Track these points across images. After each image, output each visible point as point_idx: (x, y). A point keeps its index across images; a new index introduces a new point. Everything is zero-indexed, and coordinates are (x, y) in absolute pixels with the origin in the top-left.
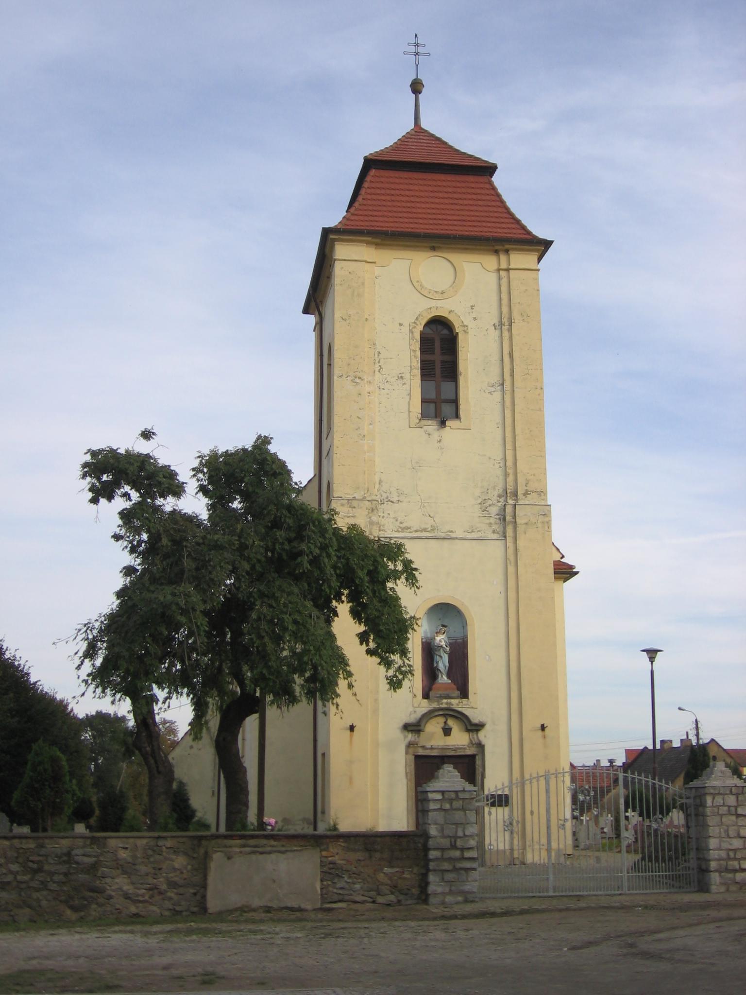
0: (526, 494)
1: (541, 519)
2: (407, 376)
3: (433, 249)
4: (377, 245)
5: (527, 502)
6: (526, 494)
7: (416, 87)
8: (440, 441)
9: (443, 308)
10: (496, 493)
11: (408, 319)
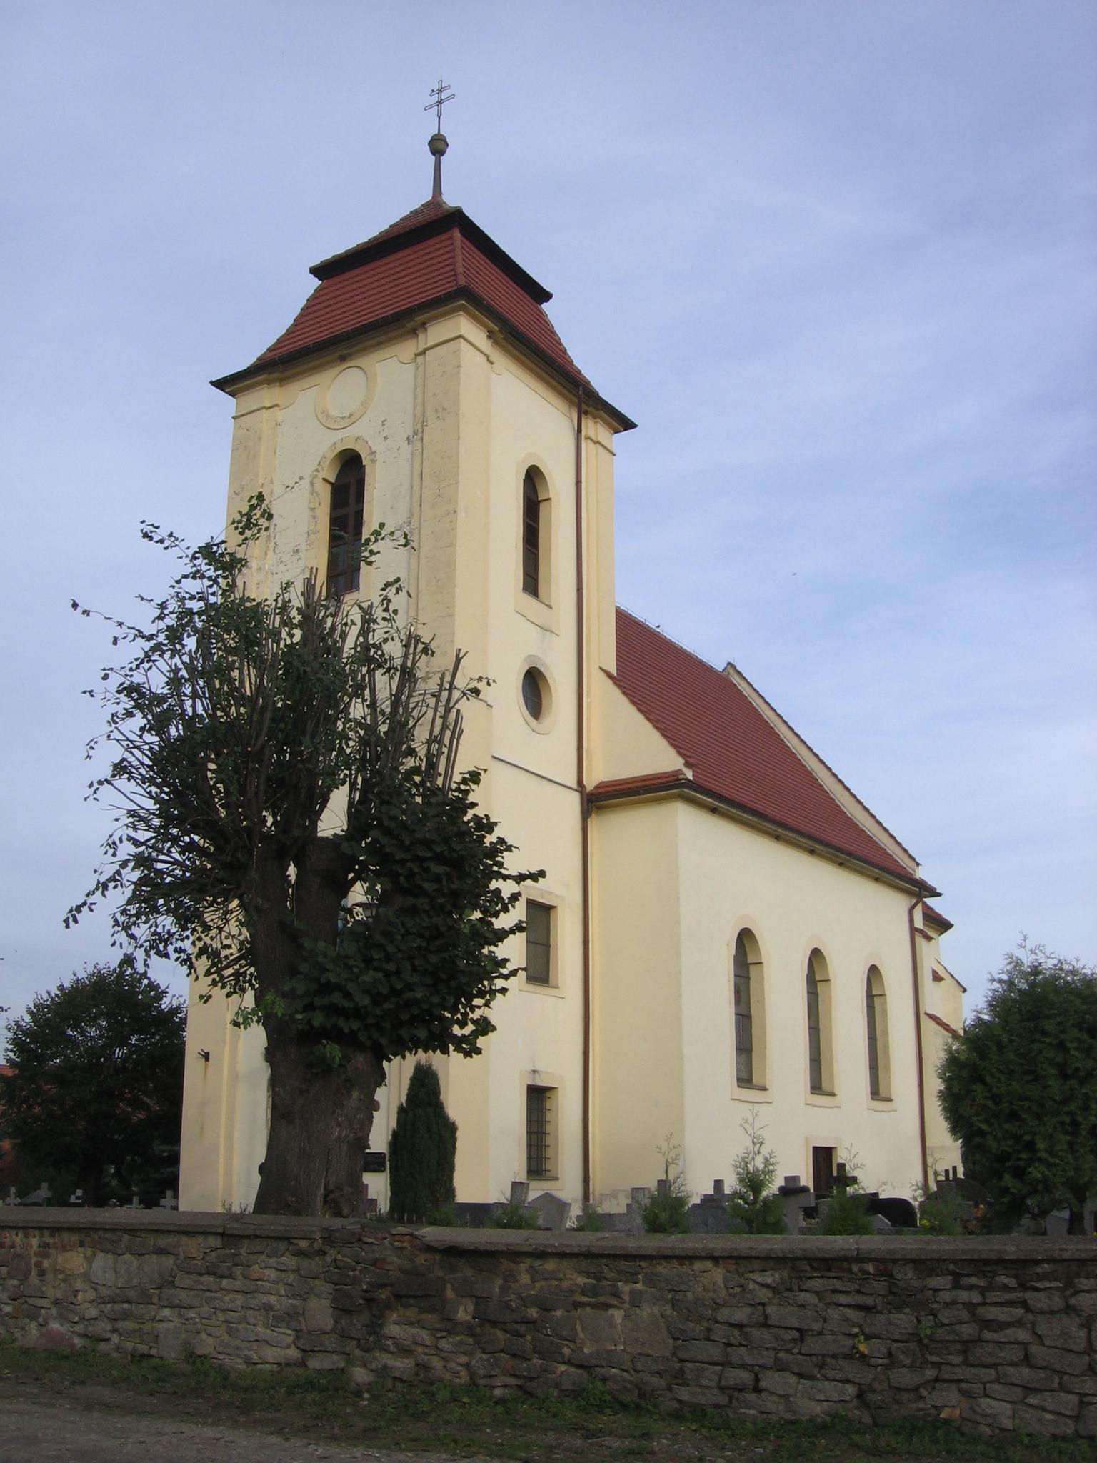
2: (303, 547)
3: (343, 359)
4: (282, 381)
7: (438, 146)
9: (345, 439)
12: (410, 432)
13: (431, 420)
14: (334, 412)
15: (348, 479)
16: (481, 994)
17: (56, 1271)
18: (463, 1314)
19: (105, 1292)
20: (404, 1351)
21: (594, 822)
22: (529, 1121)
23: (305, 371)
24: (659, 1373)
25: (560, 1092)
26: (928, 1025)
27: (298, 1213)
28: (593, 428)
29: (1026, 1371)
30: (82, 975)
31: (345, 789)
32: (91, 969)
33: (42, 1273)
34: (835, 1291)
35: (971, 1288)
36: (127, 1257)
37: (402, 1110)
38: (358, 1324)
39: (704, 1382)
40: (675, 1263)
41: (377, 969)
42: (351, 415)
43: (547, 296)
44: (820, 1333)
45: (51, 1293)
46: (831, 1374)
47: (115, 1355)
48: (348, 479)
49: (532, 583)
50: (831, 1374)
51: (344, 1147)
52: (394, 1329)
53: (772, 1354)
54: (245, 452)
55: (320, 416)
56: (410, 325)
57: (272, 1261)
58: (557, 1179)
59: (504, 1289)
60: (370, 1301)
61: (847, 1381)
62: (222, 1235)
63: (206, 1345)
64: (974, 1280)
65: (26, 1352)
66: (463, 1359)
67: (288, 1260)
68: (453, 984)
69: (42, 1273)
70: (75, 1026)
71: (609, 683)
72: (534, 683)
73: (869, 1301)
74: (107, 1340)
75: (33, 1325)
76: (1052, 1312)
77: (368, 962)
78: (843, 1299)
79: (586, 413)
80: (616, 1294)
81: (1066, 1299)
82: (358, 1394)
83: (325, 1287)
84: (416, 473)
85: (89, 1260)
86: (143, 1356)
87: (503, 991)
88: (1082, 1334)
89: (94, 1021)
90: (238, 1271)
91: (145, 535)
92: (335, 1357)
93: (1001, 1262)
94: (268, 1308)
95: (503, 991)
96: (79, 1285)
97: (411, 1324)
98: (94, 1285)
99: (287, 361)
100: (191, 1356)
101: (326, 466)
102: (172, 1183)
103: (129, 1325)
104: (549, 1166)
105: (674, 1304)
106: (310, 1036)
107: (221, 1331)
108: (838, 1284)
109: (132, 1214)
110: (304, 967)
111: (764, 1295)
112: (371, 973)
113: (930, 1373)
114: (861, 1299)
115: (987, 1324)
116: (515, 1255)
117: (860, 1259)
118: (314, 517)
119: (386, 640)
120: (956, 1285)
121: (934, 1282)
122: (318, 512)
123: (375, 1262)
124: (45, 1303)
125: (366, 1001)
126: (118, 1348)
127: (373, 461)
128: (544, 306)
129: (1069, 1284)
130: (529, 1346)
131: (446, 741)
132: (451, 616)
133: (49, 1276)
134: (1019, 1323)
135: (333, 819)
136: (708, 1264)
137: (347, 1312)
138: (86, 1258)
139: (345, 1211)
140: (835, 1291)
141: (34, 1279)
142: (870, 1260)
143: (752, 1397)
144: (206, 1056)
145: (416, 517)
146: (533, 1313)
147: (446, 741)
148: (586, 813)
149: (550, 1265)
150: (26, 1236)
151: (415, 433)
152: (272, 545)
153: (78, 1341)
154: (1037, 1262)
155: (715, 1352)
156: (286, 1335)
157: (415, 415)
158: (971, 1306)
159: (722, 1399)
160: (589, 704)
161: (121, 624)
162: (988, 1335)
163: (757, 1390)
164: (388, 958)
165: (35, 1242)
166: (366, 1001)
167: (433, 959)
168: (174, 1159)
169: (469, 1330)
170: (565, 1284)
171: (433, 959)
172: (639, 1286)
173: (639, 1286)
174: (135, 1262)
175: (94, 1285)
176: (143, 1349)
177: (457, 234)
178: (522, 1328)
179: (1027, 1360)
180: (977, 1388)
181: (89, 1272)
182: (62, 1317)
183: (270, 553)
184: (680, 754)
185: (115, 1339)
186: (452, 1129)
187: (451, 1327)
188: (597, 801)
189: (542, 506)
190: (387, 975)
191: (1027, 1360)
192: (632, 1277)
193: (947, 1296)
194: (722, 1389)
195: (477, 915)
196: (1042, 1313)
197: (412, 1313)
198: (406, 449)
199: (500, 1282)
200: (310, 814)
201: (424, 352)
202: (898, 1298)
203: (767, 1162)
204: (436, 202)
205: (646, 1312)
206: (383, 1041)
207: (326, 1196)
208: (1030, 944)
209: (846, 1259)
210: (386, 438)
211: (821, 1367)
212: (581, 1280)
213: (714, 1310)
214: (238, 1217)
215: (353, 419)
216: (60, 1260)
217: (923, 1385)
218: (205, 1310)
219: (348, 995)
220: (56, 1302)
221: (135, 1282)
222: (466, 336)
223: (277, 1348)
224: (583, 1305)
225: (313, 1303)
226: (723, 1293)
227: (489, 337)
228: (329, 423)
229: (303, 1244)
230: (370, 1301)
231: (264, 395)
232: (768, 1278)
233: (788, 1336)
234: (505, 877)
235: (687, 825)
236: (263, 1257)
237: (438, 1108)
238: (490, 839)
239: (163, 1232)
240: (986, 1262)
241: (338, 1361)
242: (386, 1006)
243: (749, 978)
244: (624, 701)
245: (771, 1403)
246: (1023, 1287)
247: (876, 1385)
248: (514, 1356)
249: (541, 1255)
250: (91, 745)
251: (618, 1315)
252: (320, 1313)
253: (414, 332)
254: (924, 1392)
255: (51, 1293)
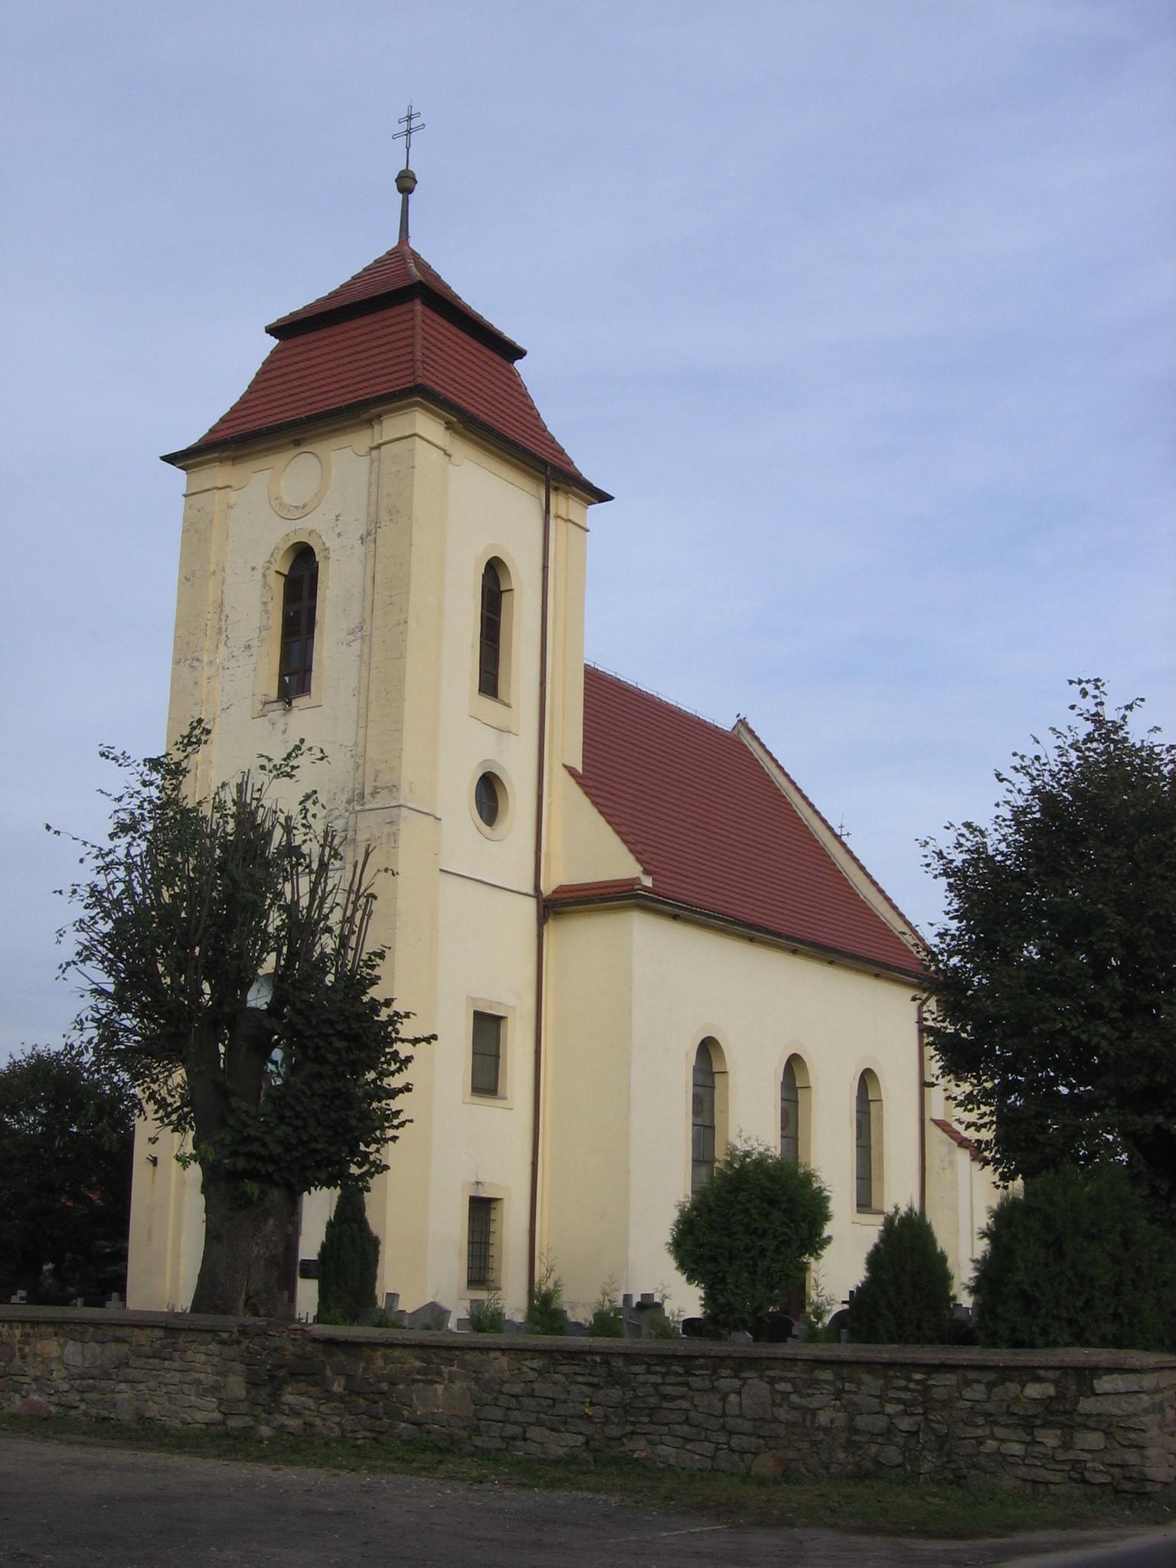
0: (374, 794)
1: (387, 829)
2: (255, 643)
3: (297, 443)
4: (235, 460)
5: (376, 806)
6: (374, 794)
7: (406, 183)
8: (284, 732)
9: (300, 530)
10: (344, 798)
11: (261, 559)
12: (363, 531)
13: (385, 519)
14: (288, 500)
15: (301, 573)
16: (377, 1141)
17: (36, 1355)
18: (337, 1387)
19: (75, 1371)
20: (297, 1414)
21: (551, 929)
22: (472, 1231)
23: (259, 451)
24: (464, 1428)
25: (505, 1202)
26: (934, 1133)
27: (224, 1313)
28: (562, 504)
29: (686, 1428)
30: (19, 1057)
31: (274, 955)
32: (28, 1051)
33: (24, 1357)
34: (576, 1374)
35: (656, 1373)
36: (93, 1344)
37: (330, 1225)
38: (263, 1394)
39: (492, 1434)
40: (477, 1352)
41: (287, 1124)
42: (305, 506)
43: (520, 354)
44: (565, 1402)
45: (31, 1372)
46: (571, 1428)
47: (83, 1418)
48: (301, 573)
49: (489, 683)
50: (571, 1428)
51: (262, 1263)
52: (288, 1398)
53: (535, 1415)
54: (196, 535)
55: (273, 502)
56: (365, 416)
57: (202, 1348)
58: (499, 1289)
59: (365, 1370)
60: (272, 1377)
61: (580, 1433)
62: (165, 1328)
63: (152, 1410)
64: (658, 1368)
65: (14, 1416)
66: (337, 1419)
67: (214, 1347)
68: (348, 1136)
69: (24, 1357)
70: (11, 1114)
71: (571, 781)
72: (489, 792)
73: (595, 1380)
74: (77, 1407)
75: (17, 1396)
76: (705, 1391)
77: (281, 1119)
78: (580, 1379)
79: (556, 489)
80: (440, 1374)
81: (712, 1382)
82: (261, 1442)
83: (241, 1367)
84: (369, 576)
85: (62, 1346)
86: (105, 1419)
87: (394, 1138)
88: (720, 1405)
89: (31, 1108)
90: (176, 1355)
91: (102, 755)
92: (247, 1418)
93: (674, 1357)
94: (199, 1382)
95: (394, 1138)
96: (53, 1366)
97: (301, 1394)
98: (66, 1366)
99: (236, 440)
100: (141, 1418)
101: (279, 556)
102: (119, 1284)
103: (94, 1396)
104: (492, 1276)
105: (477, 1380)
106: (235, 1176)
107: (164, 1400)
108: (577, 1369)
109: (79, 1311)
110: (231, 1121)
111: (532, 1375)
112: (283, 1127)
113: (629, 1428)
114: (591, 1379)
115: (665, 1397)
116: (373, 1345)
117: (591, 1353)
118: (266, 612)
119: (304, 842)
120: (648, 1372)
121: (635, 1369)
122: (270, 606)
123: (276, 1350)
124: (27, 1380)
125: (278, 1150)
126: (85, 1413)
127: (327, 558)
128: (518, 365)
129: (715, 1372)
130: (381, 1410)
131: (357, 921)
132: (399, 731)
133: (30, 1359)
134: (683, 1397)
135: (258, 998)
136: (498, 1354)
137: (256, 1385)
138: (60, 1345)
139: (262, 1312)
140: (576, 1374)
141: (17, 1361)
142: (598, 1353)
143: (520, 1443)
144: (154, 1161)
145: (368, 621)
146: (385, 1386)
147: (357, 921)
148: (542, 919)
149: (397, 1353)
150: (11, 1328)
151: (369, 534)
152: (223, 638)
153: (52, 1408)
154: (697, 1358)
155: (499, 1414)
156: (211, 1402)
157: (369, 514)
158: (656, 1385)
159: (503, 1445)
160: (550, 804)
161: (85, 843)
162: (665, 1405)
163: (525, 1439)
164: (297, 1116)
165: (18, 1332)
166: (278, 1150)
167: (333, 1115)
168: (122, 1256)
169: (341, 1398)
170: (406, 1366)
171: (333, 1115)
172: (454, 1368)
173: (454, 1368)
174: (97, 1348)
175: (66, 1366)
176: (104, 1413)
177: (418, 307)
178: (377, 1397)
179: (687, 1421)
180: (656, 1438)
181: (60, 1356)
182: (40, 1391)
183: (221, 646)
184: (639, 860)
185: (83, 1406)
186: (375, 1243)
187: (329, 1396)
188: (554, 906)
189: (504, 596)
190: (296, 1128)
191: (687, 1421)
192: (450, 1362)
193: (641, 1378)
194: (502, 1438)
195: (371, 1075)
196: (698, 1390)
197: (302, 1387)
198: (359, 549)
199: (363, 1364)
200: (244, 982)
201: (378, 447)
202: (614, 1379)
203: (556, 1284)
204: (401, 255)
205: (459, 1386)
206: (293, 1180)
207: (246, 1301)
208: (745, 1135)
209: (582, 1352)
210: (339, 535)
211: (565, 1423)
212: (418, 1364)
213: (650, 1415)
214: (177, 1315)
215: (307, 509)
216: (39, 1346)
217: (625, 1435)
218: (152, 1384)
219: (264, 1145)
220: (36, 1379)
221: (99, 1363)
222: (421, 433)
223: (204, 1412)
224: (418, 1381)
225: (232, 1379)
226: (507, 1374)
227: (447, 428)
228: (279, 508)
229: (225, 1335)
230: (272, 1377)
231: (217, 474)
232: (535, 1364)
233: (545, 1403)
234: (403, 1041)
235: (644, 933)
236: (194, 1345)
237: (363, 1223)
238: (384, 1015)
239: (120, 1325)
240: (666, 1356)
241: (248, 1421)
242: (295, 1154)
243: (713, 1087)
244: (585, 802)
245: (532, 1448)
246: (688, 1373)
247: (596, 1436)
248: (371, 1417)
249: (391, 1345)
250: (61, 933)
251: (440, 1388)
252: (236, 1386)
253: (369, 423)
254: (625, 1441)
255: (31, 1372)
